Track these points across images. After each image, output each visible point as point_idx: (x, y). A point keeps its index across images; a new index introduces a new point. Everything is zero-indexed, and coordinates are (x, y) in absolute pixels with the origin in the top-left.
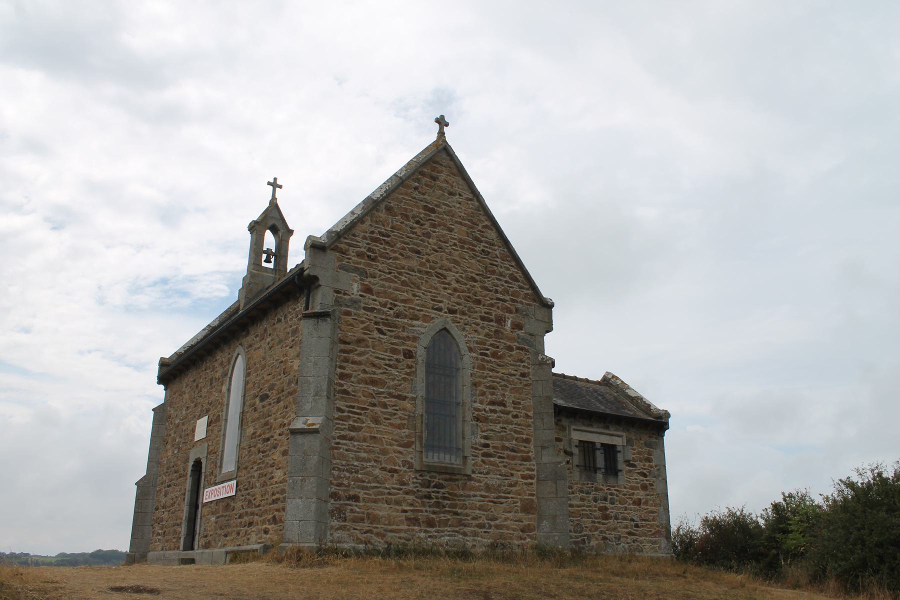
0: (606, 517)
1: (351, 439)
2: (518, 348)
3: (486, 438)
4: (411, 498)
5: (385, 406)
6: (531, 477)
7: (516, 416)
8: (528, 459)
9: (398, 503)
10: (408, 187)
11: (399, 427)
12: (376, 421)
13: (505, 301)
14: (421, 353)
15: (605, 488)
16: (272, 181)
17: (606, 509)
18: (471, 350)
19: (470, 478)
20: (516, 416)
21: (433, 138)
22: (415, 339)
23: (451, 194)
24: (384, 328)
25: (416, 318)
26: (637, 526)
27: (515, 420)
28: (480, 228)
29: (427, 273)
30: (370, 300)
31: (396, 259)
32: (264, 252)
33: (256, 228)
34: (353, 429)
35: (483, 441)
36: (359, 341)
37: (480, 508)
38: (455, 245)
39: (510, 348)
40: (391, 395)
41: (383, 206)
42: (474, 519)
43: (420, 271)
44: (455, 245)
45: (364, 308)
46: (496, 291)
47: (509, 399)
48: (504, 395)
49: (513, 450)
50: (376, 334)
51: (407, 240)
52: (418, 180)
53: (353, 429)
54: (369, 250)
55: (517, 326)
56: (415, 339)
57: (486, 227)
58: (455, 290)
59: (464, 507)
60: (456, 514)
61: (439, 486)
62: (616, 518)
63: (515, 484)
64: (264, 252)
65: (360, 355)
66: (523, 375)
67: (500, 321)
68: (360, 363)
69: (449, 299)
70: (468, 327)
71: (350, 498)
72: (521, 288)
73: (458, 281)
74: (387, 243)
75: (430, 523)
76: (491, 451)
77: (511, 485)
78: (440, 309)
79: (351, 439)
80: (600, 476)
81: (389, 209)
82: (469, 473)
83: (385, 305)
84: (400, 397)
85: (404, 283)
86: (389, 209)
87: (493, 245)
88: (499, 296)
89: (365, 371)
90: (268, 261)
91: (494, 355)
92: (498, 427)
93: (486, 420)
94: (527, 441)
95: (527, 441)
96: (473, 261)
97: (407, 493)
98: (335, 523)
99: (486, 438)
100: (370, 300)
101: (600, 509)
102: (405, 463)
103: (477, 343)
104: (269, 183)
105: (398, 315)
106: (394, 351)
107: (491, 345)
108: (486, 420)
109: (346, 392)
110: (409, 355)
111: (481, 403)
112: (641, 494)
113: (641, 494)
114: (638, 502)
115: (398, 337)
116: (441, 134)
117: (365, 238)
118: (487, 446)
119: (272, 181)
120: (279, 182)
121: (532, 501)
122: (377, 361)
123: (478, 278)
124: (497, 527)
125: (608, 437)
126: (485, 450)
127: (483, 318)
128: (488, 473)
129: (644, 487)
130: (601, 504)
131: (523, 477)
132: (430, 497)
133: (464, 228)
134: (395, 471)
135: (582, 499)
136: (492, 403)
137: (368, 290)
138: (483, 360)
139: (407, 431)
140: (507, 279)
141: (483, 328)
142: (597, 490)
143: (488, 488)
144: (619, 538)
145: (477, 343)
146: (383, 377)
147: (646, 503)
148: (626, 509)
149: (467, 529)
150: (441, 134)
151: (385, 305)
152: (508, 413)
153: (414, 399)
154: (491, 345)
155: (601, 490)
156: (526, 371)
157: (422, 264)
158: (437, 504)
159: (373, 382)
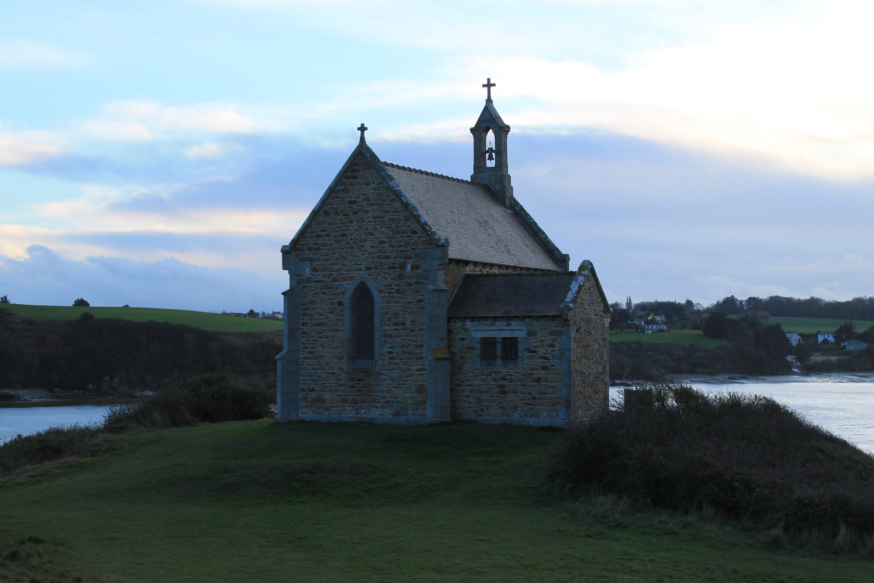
0: (504, 392)
1: (310, 358)
2: (415, 283)
3: (391, 347)
4: (342, 388)
5: (327, 337)
6: (424, 370)
7: (413, 331)
8: (421, 358)
9: (336, 391)
10: (338, 191)
11: (336, 348)
12: (323, 346)
13: (406, 251)
14: (347, 300)
15: (504, 371)
16: (492, 82)
17: (504, 386)
18: (381, 292)
19: (380, 374)
20: (413, 331)
21: (357, 143)
22: (344, 293)
23: (367, 184)
24: (325, 291)
25: (344, 280)
26: (534, 398)
27: (412, 333)
28: (388, 202)
29: (351, 248)
30: (318, 276)
31: (331, 244)
32: (487, 152)
33: (478, 132)
34: (310, 353)
35: (389, 350)
36: (312, 302)
37: (387, 391)
38: (370, 221)
39: (410, 284)
40: (331, 330)
41: (322, 212)
42: (383, 398)
43: (346, 248)
44: (370, 221)
45: (314, 282)
46: (400, 246)
47: (408, 319)
48: (404, 318)
49: (410, 353)
50: (321, 295)
51: (338, 229)
52: (344, 184)
53: (310, 353)
54: (315, 244)
55: (415, 267)
56: (344, 293)
57: (393, 200)
58: (370, 253)
59: (376, 391)
60: (371, 395)
61: (360, 380)
62: (514, 393)
63: (411, 375)
64: (487, 152)
65: (312, 310)
66: (420, 301)
67: (403, 266)
68: (312, 315)
69: (366, 261)
70: (379, 277)
71: (310, 390)
72: (419, 237)
73: (372, 247)
74: (326, 236)
75: (356, 402)
76: (394, 355)
77: (408, 376)
78: (360, 270)
79: (310, 358)
80: (499, 362)
81: (326, 212)
82: (378, 370)
83: (325, 276)
84: (335, 330)
85: (337, 259)
86: (326, 212)
87: (398, 212)
88: (402, 249)
89: (315, 319)
90: (491, 158)
91: (398, 292)
92: (399, 340)
93: (390, 336)
94: (421, 346)
95: (421, 346)
96: (383, 229)
97: (341, 385)
98: (303, 404)
99: (391, 347)
100: (318, 276)
101: (499, 387)
102: (339, 368)
103: (385, 286)
104: (489, 80)
105: (334, 281)
106: (332, 303)
107: (396, 285)
108: (390, 336)
109: (305, 333)
110: (340, 304)
111: (388, 325)
112: (541, 374)
113: (541, 374)
114: (538, 380)
115: (333, 294)
116: (362, 139)
117: (312, 237)
118: (391, 353)
119: (492, 82)
120: (486, 83)
121: (424, 385)
122: (322, 312)
123: (386, 240)
124: (398, 402)
125: (509, 332)
126: (390, 355)
127: (390, 268)
128: (392, 370)
129: (545, 368)
130: (501, 383)
131: (418, 370)
132: (354, 387)
133: (376, 207)
134: (334, 373)
135: (483, 380)
136: (396, 324)
137: (315, 270)
138: (389, 297)
139: (340, 350)
140: (409, 234)
141: (390, 275)
142: (496, 372)
143: (392, 379)
144: (516, 407)
145: (385, 286)
146: (325, 320)
147: (546, 380)
148: (524, 386)
149: (378, 405)
150: (362, 139)
151: (325, 276)
152: (407, 329)
153: (343, 330)
154: (396, 285)
155: (500, 372)
156: (422, 298)
157: (348, 243)
158: (359, 391)
159: (321, 324)
